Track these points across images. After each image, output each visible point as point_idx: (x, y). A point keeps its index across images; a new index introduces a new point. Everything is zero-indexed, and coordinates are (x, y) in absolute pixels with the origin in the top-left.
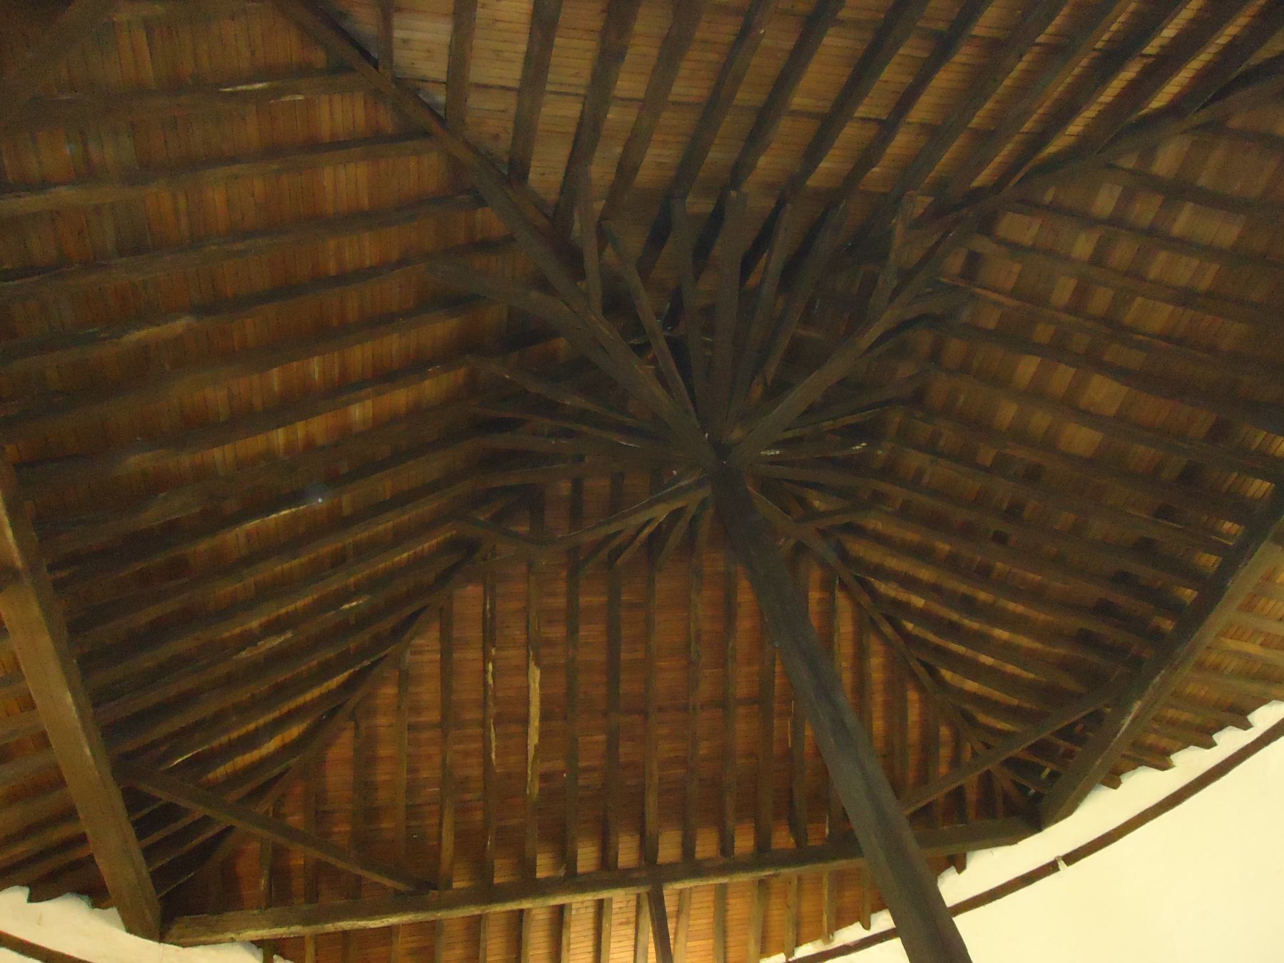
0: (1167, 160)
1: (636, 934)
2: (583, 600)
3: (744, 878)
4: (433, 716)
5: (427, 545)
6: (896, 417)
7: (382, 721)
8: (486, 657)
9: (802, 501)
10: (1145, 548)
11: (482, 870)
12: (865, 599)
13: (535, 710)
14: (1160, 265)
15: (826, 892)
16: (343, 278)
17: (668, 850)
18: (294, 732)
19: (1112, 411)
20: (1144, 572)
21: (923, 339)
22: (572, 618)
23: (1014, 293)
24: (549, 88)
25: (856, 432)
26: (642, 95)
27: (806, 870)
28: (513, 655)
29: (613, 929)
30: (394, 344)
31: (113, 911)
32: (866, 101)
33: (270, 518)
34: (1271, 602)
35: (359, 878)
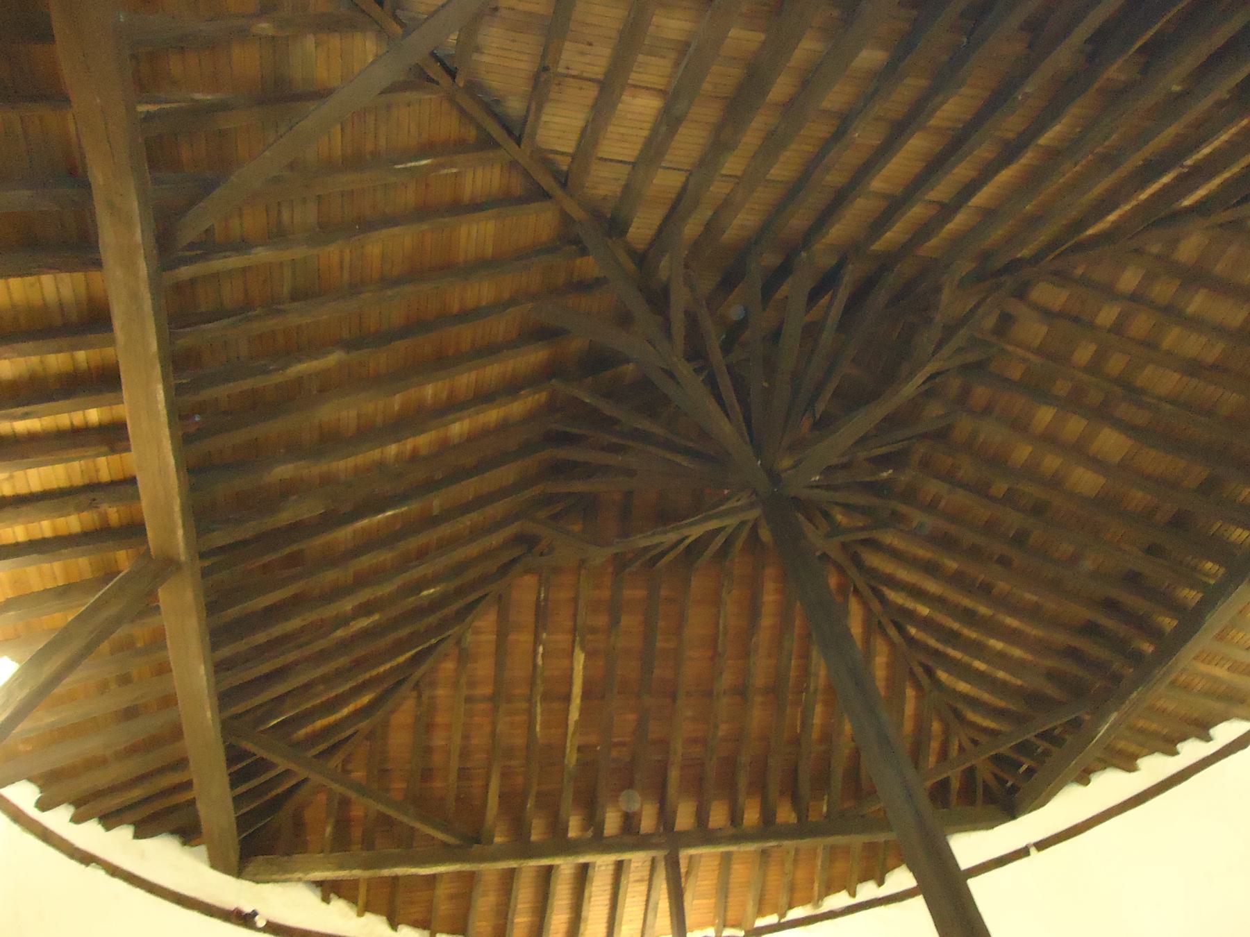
0: (1190, 247)
1: (649, 890)
3: (751, 847)
5: (496, 539)
7: (441, 692)
8: (537, 641)
9: (827, 515)
10: (1132, 579)
11: (519, 828)
12: (876, 606)
13: (577, 690)
14: (1172, 337)
15: (819, 862)
16: (466, 315)
17: (684, 819)
18: (365, 699)
19: (1117, 459)
22: (614, 609)
23: (1039, 351)
26: (739, 173)
27: (806, 843)
28: (561, 639)
29: (629, 885)
30: (493, 371)
31: (202, 850)
34: (1240, 633)
35: (412, 828)
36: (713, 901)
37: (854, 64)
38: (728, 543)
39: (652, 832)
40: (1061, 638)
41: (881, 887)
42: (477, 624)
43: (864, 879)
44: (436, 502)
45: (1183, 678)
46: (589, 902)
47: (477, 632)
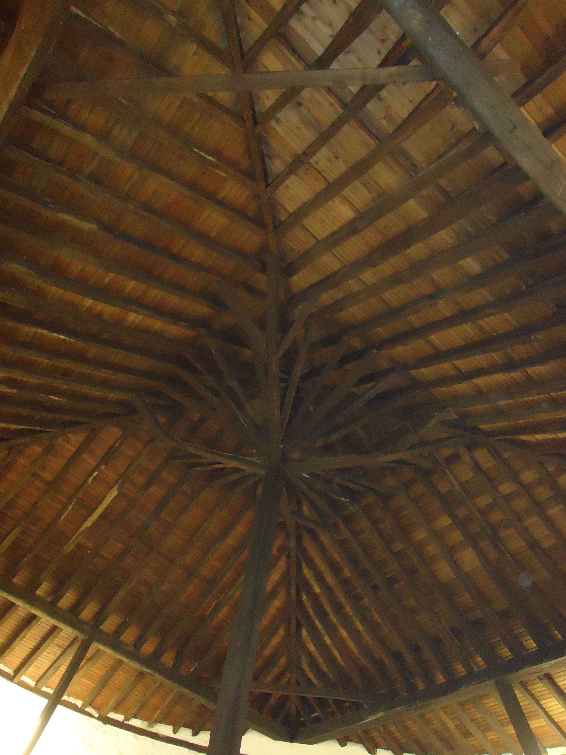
2: (164, 474)
3: (136, 666)
4: (48, 476)
5: (113, 396)
6: (370, 499)
7: (22, 461)
8: (97, 467)
9: (299, 503)
10: (436, 642)
12: (294, 571)
13: (100, 510)
14: (532, 521)
15: (169, 699)
16: (176, 258)
17: (109, 625)
20: (428, 654)
21: (409, 474)
22: (152, 479)
23: (461, 484)
24: (333, 251)
25: (347, 492)
27: (169, 683)
32: (462, 360)
33: (53, 334)
36: (94, 685)
37: (461, 262)
38: (237, 483)
39: (85, 621)
40: (380, 653)
41: (194, 737)
42: (70, 436)
43: (187, 726)
44: (94, 351)
45: (430, 715)
46: (22, 640)
47: (68, 441)
